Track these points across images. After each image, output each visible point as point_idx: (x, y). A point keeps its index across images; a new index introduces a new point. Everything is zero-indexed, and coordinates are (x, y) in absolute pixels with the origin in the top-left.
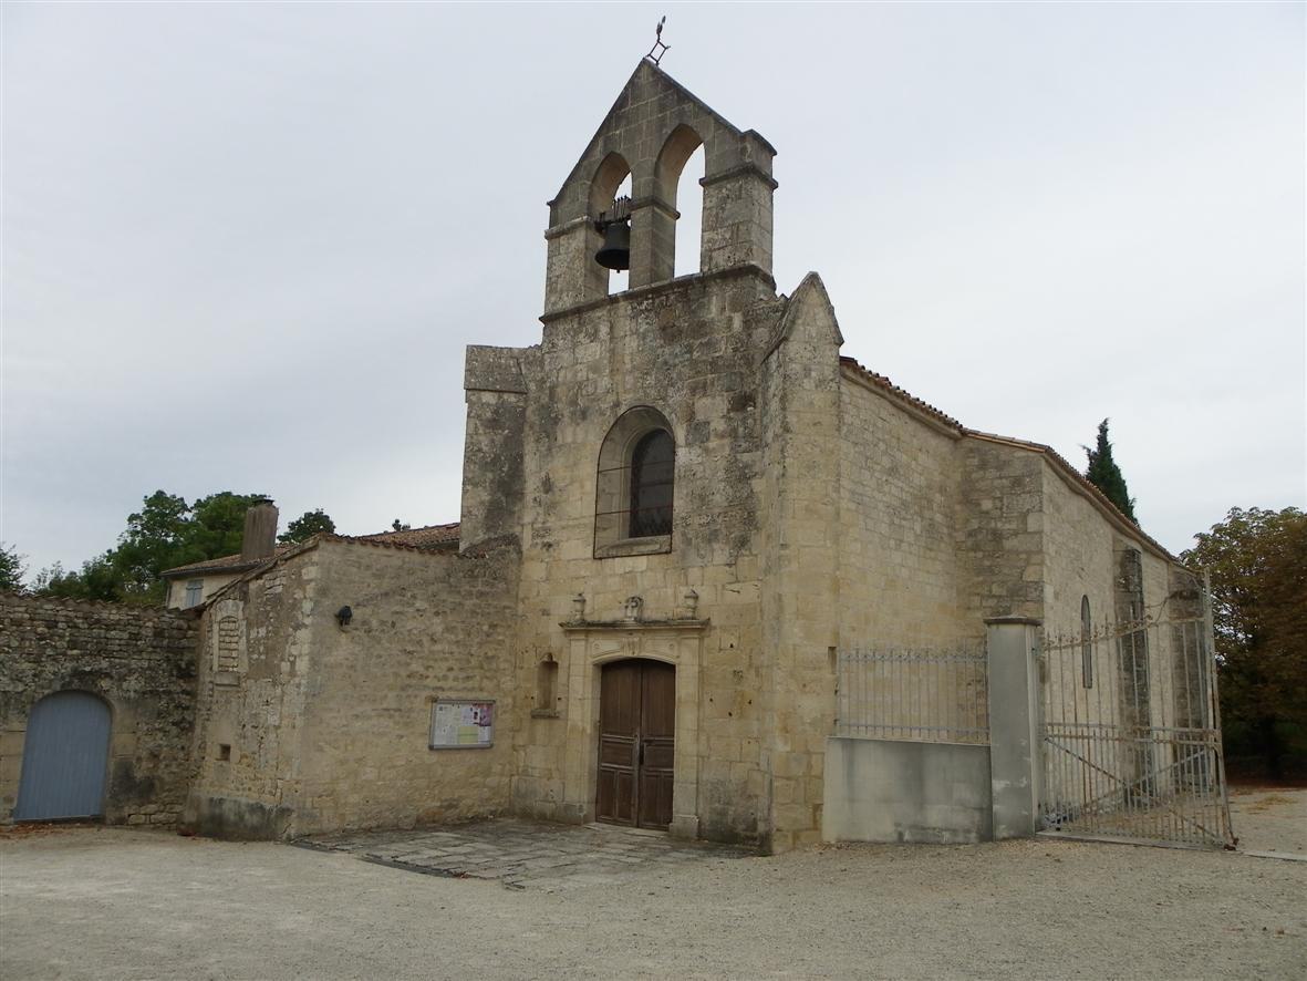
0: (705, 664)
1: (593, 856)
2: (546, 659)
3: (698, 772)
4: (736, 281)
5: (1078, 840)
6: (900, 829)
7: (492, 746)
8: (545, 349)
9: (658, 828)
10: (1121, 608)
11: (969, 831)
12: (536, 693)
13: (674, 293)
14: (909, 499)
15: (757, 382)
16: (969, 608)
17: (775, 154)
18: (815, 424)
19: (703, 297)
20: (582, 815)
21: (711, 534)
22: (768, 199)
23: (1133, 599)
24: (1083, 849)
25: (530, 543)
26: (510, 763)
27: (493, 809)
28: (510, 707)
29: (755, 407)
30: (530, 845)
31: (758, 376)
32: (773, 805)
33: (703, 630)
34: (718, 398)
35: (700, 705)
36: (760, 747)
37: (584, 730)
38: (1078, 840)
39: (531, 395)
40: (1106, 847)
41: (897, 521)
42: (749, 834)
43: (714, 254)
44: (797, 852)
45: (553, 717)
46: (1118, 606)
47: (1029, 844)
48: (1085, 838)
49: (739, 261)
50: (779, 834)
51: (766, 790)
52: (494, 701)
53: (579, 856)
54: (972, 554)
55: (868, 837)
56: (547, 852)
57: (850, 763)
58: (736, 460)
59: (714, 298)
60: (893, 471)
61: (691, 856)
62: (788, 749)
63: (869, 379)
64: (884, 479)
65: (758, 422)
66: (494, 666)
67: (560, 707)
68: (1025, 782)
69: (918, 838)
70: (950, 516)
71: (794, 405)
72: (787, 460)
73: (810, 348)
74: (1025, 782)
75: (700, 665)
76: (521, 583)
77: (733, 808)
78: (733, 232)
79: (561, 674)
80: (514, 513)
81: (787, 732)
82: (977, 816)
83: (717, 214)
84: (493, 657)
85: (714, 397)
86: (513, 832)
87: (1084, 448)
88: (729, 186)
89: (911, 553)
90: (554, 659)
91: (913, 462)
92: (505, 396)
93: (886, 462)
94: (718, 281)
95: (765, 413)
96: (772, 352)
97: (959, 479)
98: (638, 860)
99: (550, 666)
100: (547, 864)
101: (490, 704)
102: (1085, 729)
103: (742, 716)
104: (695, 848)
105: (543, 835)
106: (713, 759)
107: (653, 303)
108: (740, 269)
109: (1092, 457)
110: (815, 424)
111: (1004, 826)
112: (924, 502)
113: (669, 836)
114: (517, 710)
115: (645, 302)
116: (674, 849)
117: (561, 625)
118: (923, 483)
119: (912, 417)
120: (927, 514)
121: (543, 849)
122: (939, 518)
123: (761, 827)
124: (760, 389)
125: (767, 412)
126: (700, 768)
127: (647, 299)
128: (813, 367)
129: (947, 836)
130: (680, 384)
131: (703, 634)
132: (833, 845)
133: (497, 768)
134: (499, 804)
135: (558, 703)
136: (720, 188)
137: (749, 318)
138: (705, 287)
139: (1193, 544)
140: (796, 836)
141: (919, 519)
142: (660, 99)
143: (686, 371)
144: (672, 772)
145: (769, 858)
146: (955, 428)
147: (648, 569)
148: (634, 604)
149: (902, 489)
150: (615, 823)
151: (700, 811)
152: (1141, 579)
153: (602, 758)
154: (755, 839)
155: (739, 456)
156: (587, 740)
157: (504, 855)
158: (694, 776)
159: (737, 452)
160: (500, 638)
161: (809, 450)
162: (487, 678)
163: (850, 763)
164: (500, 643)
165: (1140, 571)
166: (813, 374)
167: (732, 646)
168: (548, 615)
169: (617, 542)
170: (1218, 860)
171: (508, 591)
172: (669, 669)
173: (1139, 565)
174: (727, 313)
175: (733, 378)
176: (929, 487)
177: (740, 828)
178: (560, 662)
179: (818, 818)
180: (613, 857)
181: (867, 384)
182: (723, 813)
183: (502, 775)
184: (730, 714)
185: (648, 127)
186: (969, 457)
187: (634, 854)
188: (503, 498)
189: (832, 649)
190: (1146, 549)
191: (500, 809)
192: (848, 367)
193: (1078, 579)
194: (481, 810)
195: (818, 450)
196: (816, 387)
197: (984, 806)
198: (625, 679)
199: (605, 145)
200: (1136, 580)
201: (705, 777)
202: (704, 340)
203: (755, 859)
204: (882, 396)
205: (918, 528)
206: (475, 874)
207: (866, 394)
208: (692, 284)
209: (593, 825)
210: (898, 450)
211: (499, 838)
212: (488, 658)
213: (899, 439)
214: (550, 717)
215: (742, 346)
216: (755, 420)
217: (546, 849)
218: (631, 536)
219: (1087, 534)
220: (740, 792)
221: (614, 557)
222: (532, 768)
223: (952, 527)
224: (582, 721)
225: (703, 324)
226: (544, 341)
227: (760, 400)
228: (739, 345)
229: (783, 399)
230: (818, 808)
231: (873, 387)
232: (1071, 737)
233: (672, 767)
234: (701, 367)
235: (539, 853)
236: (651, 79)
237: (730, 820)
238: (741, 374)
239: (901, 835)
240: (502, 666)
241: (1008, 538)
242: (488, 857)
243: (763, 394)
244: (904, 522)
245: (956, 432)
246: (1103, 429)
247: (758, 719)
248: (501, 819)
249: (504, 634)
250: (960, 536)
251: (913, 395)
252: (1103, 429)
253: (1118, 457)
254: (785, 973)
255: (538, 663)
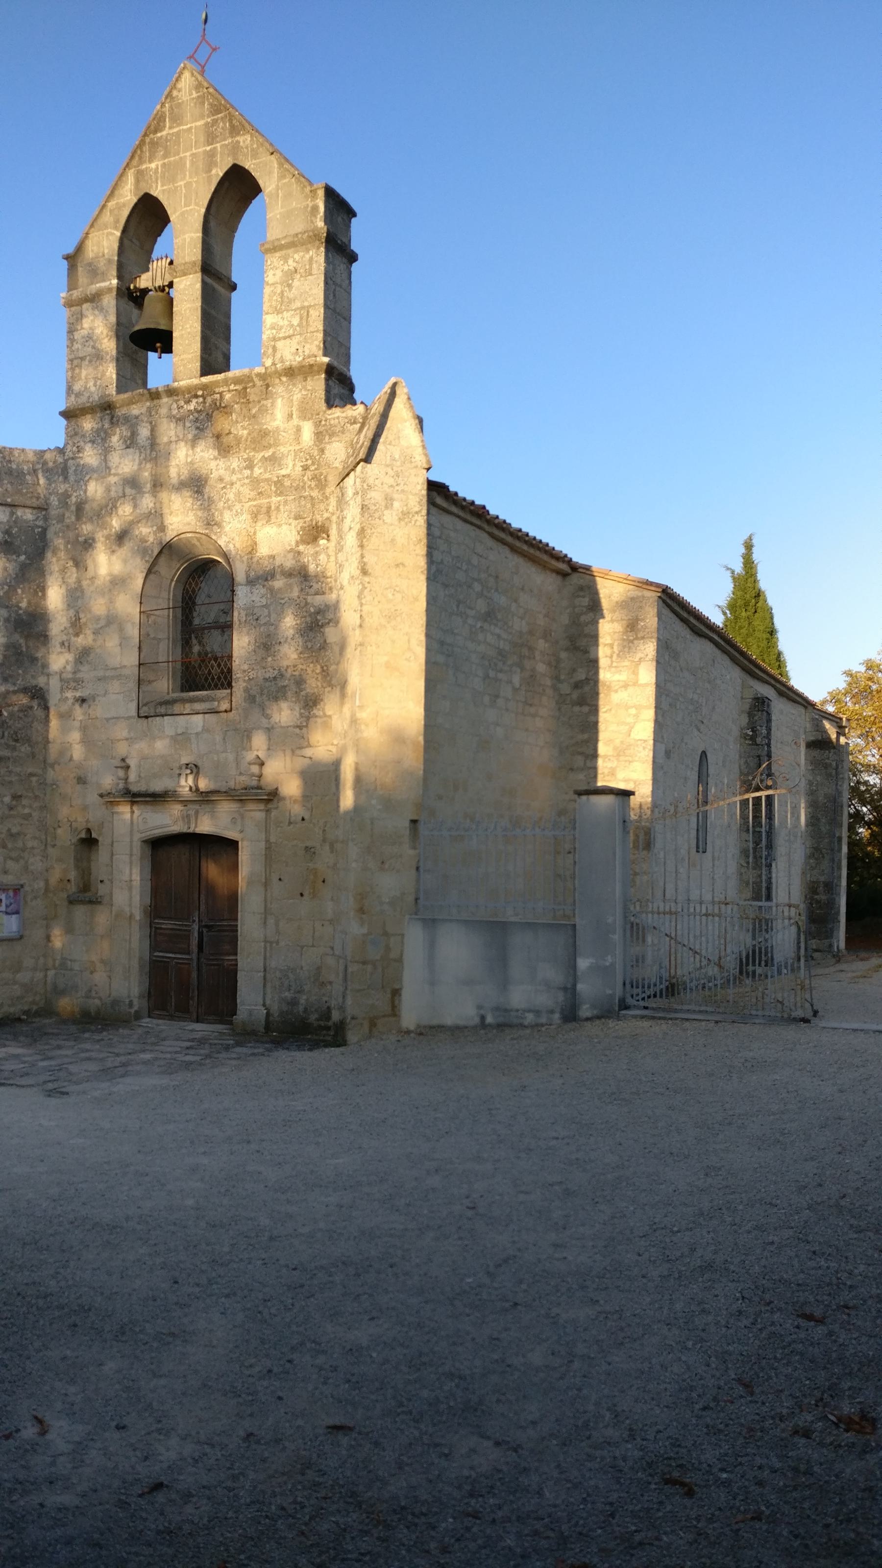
0: (273, 839)
1: (147, 1056)
2: (83, 835)
3: (265, 959)
4: (305, 380)
5: (660, 1018)
6: (482, 1012)
7: (21, 937)
8: (69, 454)
9: (221, 1022)
10: (746, 762)
11: (552, 1012)
12: (73, 875)
13: (229, 391)
14: (507, 648)
15: (331, 510)
16: (572, 769)
17: (354, 215)
18: (397, 566)
19: (267, 399)
20: (133, 1011)
21: (277, 692)
22: (345, 276)
23: (759, 752)
24: (664, 1027)
25: (59, 696)
26: (45, 956)
27: (26, 1008)
28: (43, 891)
29: (328, 540)
30: (72, 1047)
31: (333, 502)
32: (348, 992)
33: (269, 801)
34: (284, 527)
35: (266, 884)
36: (334, 931)
37: (131, 916)
38: (660, 1018)
39: (53, 512)
40: (687, 1024)
41: (492, 674)
42: (322, 1023)
43: (280, 344)
44: (373, 1040)
45: (95, 902)
46: (743, 761)
47: (611, 1023)
48: (668, 1016)
49: (309, 357)
50: (354, 1022)
51: (341, 975)
52: (22, 886)
53: (129, 1057)
54: (577, 709)
55: (449, 1021)
56: (94, 1055)
57: (432, 945)
58: (307, 604)
59: (279, 400)
60: (489, 616)
61: (256, 1051)
62: (365, 930)
63: (463, 508)
64: (479, 625)
65: (332, 559)
66: (20, 844)
67: (102, 890)
68: (609, 959)
69: (501, 1020)
70: (555, 664)
71: (373, 543)
72: (365, 608)
73: (391, 473)
74: (609, 959)
75: (267, 841)
76: (50, 745)
77: (305, 997)
78: (301, 319)
79: (102, 855)
80: (36, 659)
81: (364, 913)
82: (561, 996)
83: (282, 292)
84: (18, 834)
85: (280, 526)
86: (53, 1034)
87: (728, 569)
88: (296, 256)
89: (507, 710)
90: (94, 835)
91: (514, 605)
92: (19, 512)
93: (481, 606)
94: (284, 379)
95: (340, 548)
96: (348, 475)
97: (567, 622)
98: (198, 1058)
99: (89, 842)
100: (93, 1067)
101: (17, 890)
102: (673, 904)
103: (314, 895)
104: (262, 1042)
105: (87, 1035)
106: (282, 944)
107: (204, 402)
108: (311, 366)
109: (735, 579)
110: (397, 566)
111: (588, 1006)
112: (525, 651)
113: (232, 1029)
114: (51, 895)
115: (194, 401)
116: (238, 1044)
117: (101, 796)
118: (525, 629)
119: (513, 549)
120: (528, 664)
121: (87, 1051)
122: (541, 668)
123: (336, 1016)
124: (334, 518)
125: (342, 546)
126: (268, 954)
127: (196, 396)
128: (396, 496)
129: (530, 1018)
130: (238, 507)
131: (270, 806)
132: (412, 1032)
133: (28, 962)
134: (33, 1002)
135: (100, 886)
136: (285, 259)
137: (321, 429)
138: (268, 386)
139: (841, 683)
140: (373, 1024)
141: (519, 670)
142: (207, 124)
143: (246, 491)
144: (236, 960)
145: (341, 1049)
146: (564, 562)
147: (206, 730)
148: (188, 771)
149: (499, 636)
150: (171, 1017)
151: (268, 1002)
152: (769, 730)
153: (154, 947)
154: (328, 1028)
155: (309, 599)
156: (136, 927)
157: (42, 1060)
158: (262, 964)
159: (307, 594)
160: (27, 811)
161: (390, 596)
162: (11, 859)
163: (432, 945)
164: (27, 817)
165: (769, 721)
166: (396, 504)
167: (303, 819)
168: (85, 783)
169: (167, 698)
170: (790, 1033)
171: (33, 755)
172: (232, 845)
173: (769, 714)
174: (295, 421)
175: (303, 503)
176: (531, 633)
177: (313, 1018)
178: (100, 839)
179: (396, 1002)
180: (169, 1056)
181: (461, 514)
182: (294, 1002)
183: (35, 969)
184: (302, 895)
185: (192, 163)
186: (578, 596)
187: (192, 1052)
188: (22, 641)
189: (414, 822)
190: (781, 694)
191: (35, 1008)
192: (439, 494)
193: (696, 732)
194: (12, 1010)
195: (399, 596)
196: (400, 519)
197: (569, 986)
198: (181, 855)
199: (137, 181)
200: (764, 731)
201: (273, 964)
202: (268, 453)
203: (327, 1050)
204: (479, 527)
205: (516, 680)
206: (11, 1082)
207: (460, 524)
208: (252, 381)
209: (146, 1021)
210: (497, 590)
211: (35, 1041)
212: (12, 835)
213: (497, 577)
214: (91, 902)
215: (313, 464)
216: (328, 556)
217: (92, 1051)
218: (183, 690)
219: (709, 682)
220: (312, 979)
221: (163, 716)
222: (71, 960)
223: (557, 678)
224: (130, 905)
225: (265, 434)
226: (66, 444)
227: (333, 532)
228: (309, 462)
229: (362, 533)
230: (396, 993)
231: (469, 517)
232: (659, 913)
233: (236, 954)
234: (264, 487)
235: (83, 1055)
236: (195, 95)
237: (301, 1008)
238: (312, 498)
239: (483, 1018)
240: (30, 844)
241: (616, 691)
242: (25, 1062)
243: (338, 524)
244: (500, 676)
245: (563, 567)
246: (749, 546)
247: (332, 899)
248: (37, 1020)
249: (30, 807)
250: (565, 688)
251: (515, 525)
252: (749, 546)
253: (765, 582)
254: (341, 1161)
255: (74, 840)
